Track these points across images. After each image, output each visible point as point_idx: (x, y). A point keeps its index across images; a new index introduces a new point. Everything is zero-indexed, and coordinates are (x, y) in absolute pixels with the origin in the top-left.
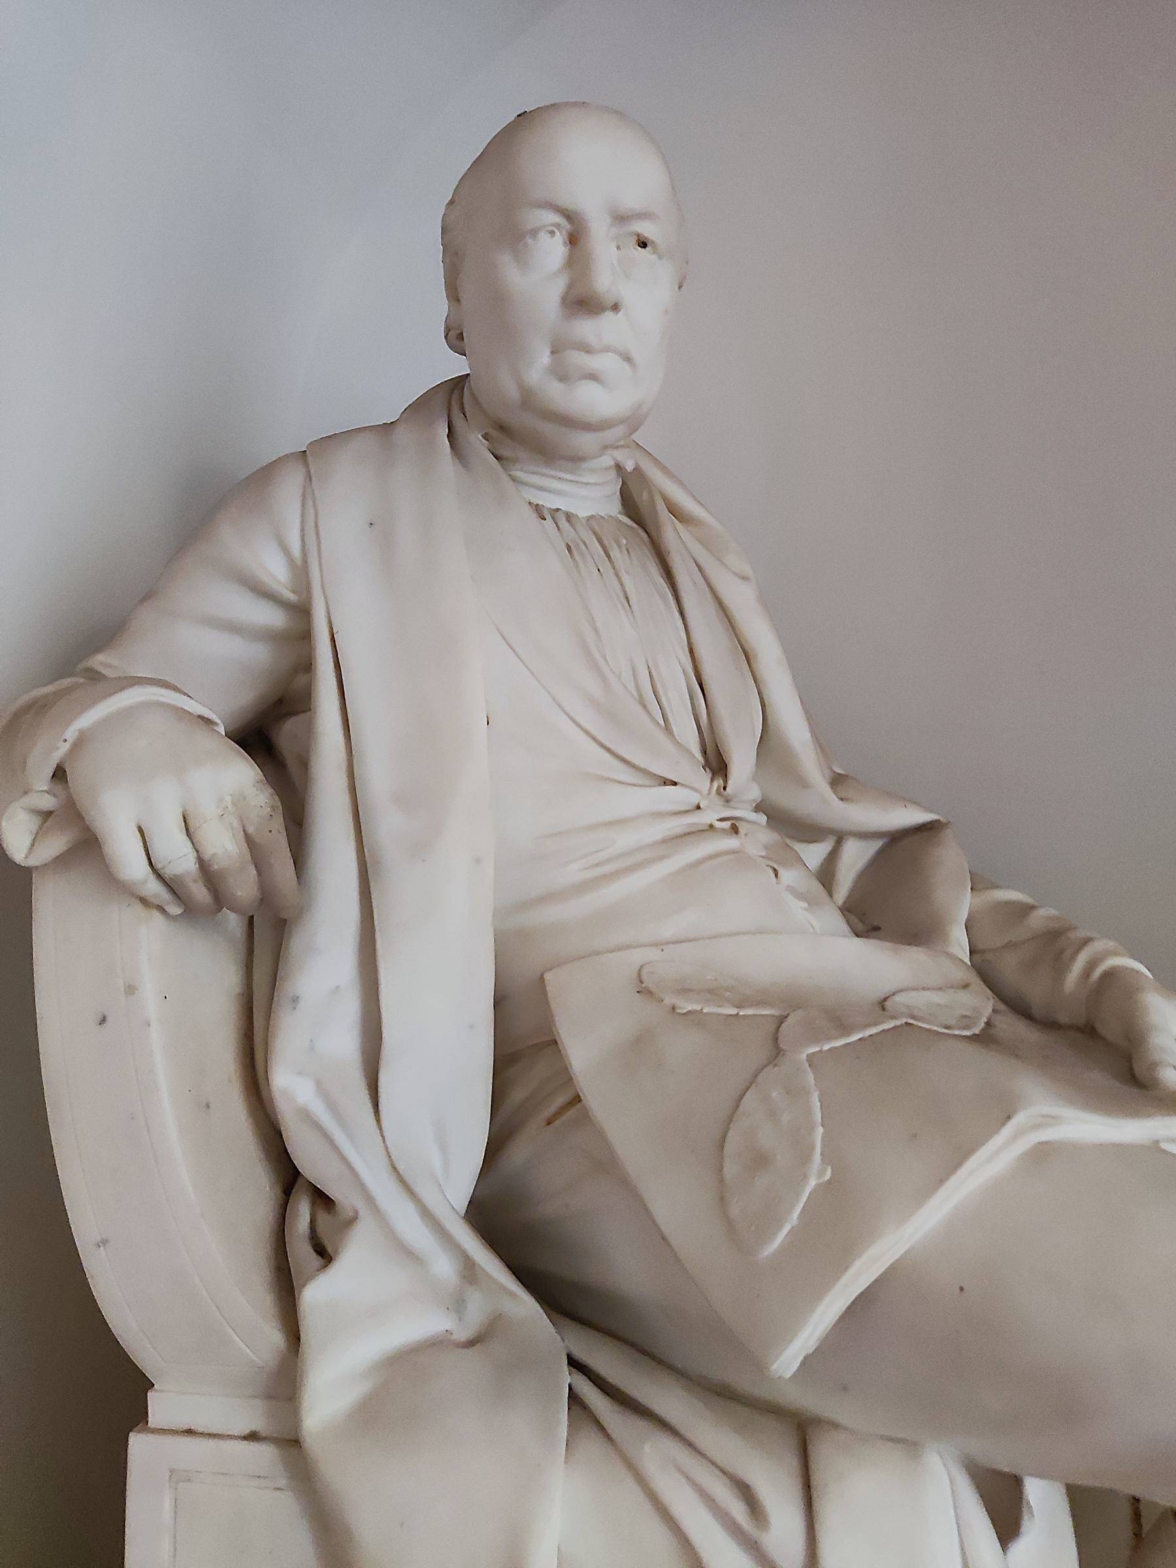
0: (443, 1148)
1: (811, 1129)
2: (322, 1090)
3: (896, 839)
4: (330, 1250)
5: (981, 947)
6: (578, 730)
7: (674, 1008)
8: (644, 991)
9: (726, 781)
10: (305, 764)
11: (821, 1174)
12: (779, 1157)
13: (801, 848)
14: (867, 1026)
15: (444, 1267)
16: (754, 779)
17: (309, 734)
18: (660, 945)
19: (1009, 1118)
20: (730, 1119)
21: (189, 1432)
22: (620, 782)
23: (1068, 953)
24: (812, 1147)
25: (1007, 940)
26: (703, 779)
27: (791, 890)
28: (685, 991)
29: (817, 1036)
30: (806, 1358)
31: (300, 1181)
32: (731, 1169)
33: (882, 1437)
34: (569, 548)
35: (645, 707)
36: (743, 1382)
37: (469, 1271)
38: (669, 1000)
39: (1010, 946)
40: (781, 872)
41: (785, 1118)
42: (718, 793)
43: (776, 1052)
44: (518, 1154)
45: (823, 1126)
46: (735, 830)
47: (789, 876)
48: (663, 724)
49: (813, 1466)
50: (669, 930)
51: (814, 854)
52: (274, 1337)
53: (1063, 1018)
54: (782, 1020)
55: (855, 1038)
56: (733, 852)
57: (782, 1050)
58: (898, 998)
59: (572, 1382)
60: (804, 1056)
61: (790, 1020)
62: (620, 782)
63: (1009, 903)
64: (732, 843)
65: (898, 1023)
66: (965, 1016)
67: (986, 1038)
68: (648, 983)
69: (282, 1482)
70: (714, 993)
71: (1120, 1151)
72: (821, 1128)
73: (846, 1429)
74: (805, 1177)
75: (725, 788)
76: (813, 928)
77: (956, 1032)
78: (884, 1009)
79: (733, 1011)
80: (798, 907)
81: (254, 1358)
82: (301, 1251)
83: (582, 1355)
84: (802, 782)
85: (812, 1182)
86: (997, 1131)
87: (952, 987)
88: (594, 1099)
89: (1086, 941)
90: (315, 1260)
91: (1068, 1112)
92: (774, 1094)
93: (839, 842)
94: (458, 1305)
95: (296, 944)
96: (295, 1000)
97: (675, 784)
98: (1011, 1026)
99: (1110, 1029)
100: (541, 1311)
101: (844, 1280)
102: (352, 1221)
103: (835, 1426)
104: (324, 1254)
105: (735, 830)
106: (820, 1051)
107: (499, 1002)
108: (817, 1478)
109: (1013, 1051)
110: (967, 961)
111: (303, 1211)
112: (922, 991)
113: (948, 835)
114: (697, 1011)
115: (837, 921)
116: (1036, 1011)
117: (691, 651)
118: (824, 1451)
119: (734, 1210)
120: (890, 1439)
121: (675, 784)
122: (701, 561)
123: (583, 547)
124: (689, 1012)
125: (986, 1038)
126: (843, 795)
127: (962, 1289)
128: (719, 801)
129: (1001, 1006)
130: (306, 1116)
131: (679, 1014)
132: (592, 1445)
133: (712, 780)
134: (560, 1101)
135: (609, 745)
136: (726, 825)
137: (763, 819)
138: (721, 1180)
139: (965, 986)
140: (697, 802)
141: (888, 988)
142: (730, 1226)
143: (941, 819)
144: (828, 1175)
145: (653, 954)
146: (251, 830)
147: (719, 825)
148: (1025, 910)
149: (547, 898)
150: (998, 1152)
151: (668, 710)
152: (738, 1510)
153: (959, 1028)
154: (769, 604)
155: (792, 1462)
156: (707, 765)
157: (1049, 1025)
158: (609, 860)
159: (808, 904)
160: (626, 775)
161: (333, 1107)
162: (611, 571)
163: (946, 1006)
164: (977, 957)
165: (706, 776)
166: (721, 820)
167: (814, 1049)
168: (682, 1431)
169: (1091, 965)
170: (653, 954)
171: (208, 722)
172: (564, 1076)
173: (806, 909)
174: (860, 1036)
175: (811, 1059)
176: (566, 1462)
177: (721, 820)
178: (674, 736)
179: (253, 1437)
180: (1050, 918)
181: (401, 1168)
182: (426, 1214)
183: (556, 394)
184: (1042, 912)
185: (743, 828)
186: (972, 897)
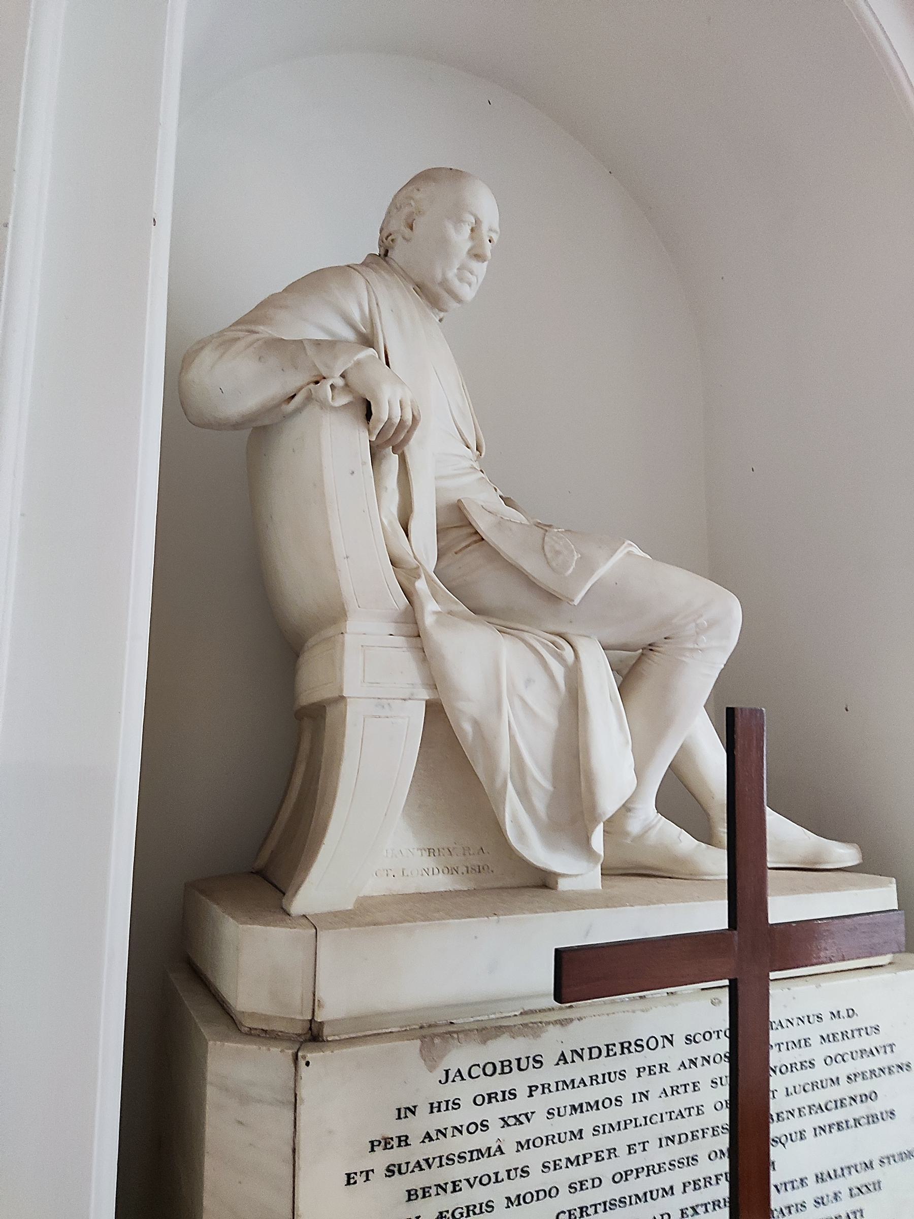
183: (456, 284)
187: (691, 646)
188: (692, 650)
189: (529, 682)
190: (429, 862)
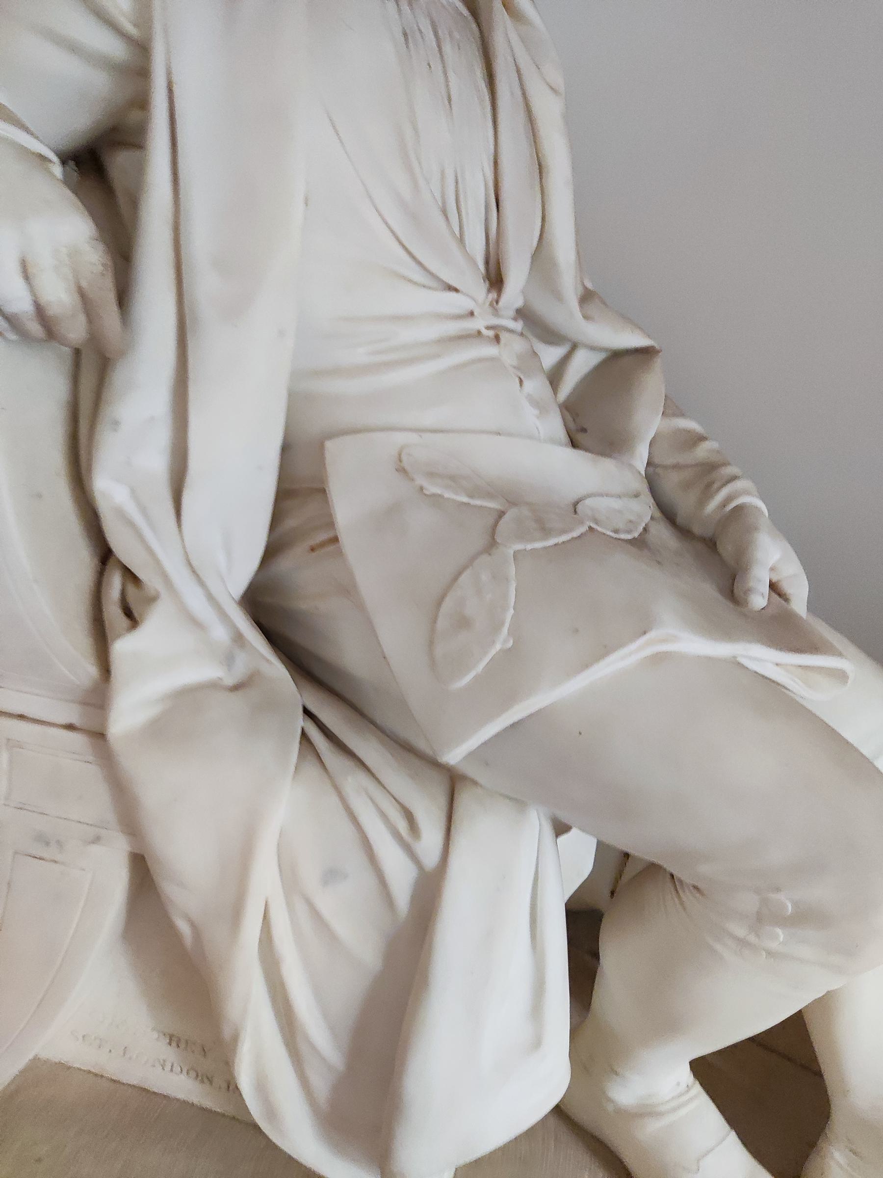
2: (133, 493)
3: (616, 356)
4: (136, 614)
5: (657, 460)
8: (402, 470)
9: (499, 295)
10: (135, 203)
11: (505, 641)
14: (564, 532)
15: (220, 634)
17: (140, 169)
19: (645, 633)
21: (21, 717)
22: (410, 281)
23: (715, 486)
24: (502, 623)
26: (479, 289)
29: (522, 535)
31: (111, 563)
32: (442, 623)
33: (502, 795)
34: (405, 35)
37: (238, 638)
39: (676, 467)
40: (526, 383)
42: (491, 305)
43: (492, 544)
44: (285, 564)
46: (497, 338)
50: (428, 419)
51: (550, 355)
52: (90, 670)
53: (697, 530)
54: (501, 514)
55: (552, 542)
56: (492, 359)
58: (588, 502)
61: (506, 517)
62: (410, 281)
63: (688, 432)
64: (491, 350)
67: (640, 543)
68: (406, 463)
69: (91, 758)
70: (453, 480)
71: (709, 660)
73: (481, 786)
74: (494, 642)
75: (497, 302)
78: (575, 512)
79: (464, 499)
80: (530, 413)
81: (72, 678)
84: (557, 295)
85: (498, 647)
88: (347, 541)
89: (733, 478)
90: (124, 621)
93: (574, 347)
94: (229, 660)
95: (119, 376)
96: (116, 423)
97: (456, 290)
98: (662, 533)
99: (726, 549)
102: (152, 599)
103: (475, 783)
104: (132, 617)
106: (525, 550)
107: (286, 449)
110: (643, 473)
111: (115, 583)
113: (658, 364)
116: (679, 520)
117: (496, 163)
118: (466, 800)
120: (510, 799)
121: (456, 290)
122: (522, 66)
123: (417, 33)
125: (640, 543)
127: (580, 733)
129: (658, 514)
130: (121, 514)
131: (425, 495)
132: (312, 770)
134: (322, 536)
135: (408, 246)
136: (491, 333)
139: (637, 496)
142: (433, 663)
143: (656, 345)
144: (510, 644)
146: (84, 284)
147: (485, 332)
148: (695, 439)
149: (337, 372)
151: (464, 220)
152: (402, 826)
154: (569, 120)
155: (442, 801)
160: (418, 275)
161: (144, 511)
162: (440, 67)
164: (651, 469)
167: (519, 546)
168: (374, 771)
171: (43, 158)
172: (331, 524)
176: (294, 777)
179: (70, 727)
181: (195, 563)
185: (504, 336)
186: (661, 420)
187: (740, 931)
188: (743, 943)
189: (331, 876)
190: (169, 1053)
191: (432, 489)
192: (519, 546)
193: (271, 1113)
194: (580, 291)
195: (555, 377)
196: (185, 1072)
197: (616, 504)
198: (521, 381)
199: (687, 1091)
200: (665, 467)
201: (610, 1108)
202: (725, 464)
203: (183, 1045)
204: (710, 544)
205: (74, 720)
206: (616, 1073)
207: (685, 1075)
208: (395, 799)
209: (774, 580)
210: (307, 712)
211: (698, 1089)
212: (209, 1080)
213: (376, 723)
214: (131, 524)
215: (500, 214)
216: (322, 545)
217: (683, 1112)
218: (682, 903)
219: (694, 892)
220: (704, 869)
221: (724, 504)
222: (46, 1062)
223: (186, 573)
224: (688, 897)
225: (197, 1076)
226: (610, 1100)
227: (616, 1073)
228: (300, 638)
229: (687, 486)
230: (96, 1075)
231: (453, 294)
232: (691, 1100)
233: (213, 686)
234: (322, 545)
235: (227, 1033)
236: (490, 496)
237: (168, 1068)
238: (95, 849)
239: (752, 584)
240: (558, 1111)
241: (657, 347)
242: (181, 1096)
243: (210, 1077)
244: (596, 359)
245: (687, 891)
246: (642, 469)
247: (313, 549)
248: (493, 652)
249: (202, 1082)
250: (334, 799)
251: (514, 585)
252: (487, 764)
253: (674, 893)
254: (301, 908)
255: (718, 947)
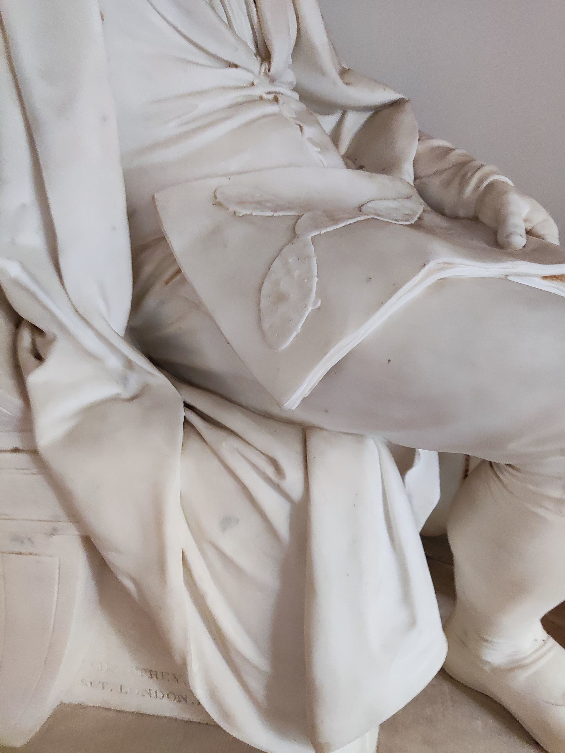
0: (105, 300)
1: (310, 279)
2: (24, 267)
4: (43, 356)
5: (421, 174)
6: (165, 23)
7: (235, 213)
8: (217, 204)
11: (315, 303)
12: (291, 296)
13: (321, 119)
16: (290, 67)
18: (228, 175)
20: (266, 275)
22: (197, 64)
23: (469, 174)
24: (310, 290)
25: (435, 170)
26: (255, 63)
27: (310, 139)
28: (242, 203)
30: (304, 398)
32: (264, 303)
35: (213, 8)
36: (275, 410)
37: (129, 365)
38: (232, 208)
40: (305, 128)
41: (297, 273)
42: (265, 74)
43: (294, 235)
45: (317, 277)
46: (276, 100)
47: (310, 131)
48: (227, 22)
49: (308, 448)
50: (233, 165)
52: (17, 402)
54: (299, 217)
56: (275, 115)
57: (297, 234)
58: (369, 205)
59: (186, 415)
60: (310, 238)
62: (197, 64)
63: (439, 147)
64: (273, 109)
65: (368, 217)
66: (407, 215)
68: (220, 198)
69: (35, 471)
70: (260, 204)
71: (483, 281)
72: (317, 278)
73: (326, 430)
75: (269, 70)
76: (323, 165)
77: (402, 223)
78: (360, 211)
79: (270, 214)
80: (314, 151)
82: (25, 356)
83: (190, 402)
84: (321, 71)
85: (310, 309)
86: (415, 274)
87: (402, 198)
89: (481, 166)
90: (33, 360)
91: (459, 260)
92: (291, 260)
94: (124, 380)
98: (433, 219)
99: (486, 217)
100: (169, 382)
101: (324, 360)
102: (53, 340)
103: (321, 429)
104: (39, 357)
105: (276, 100)
106: (320, 234)
108: (310, 455)
109: (431, 231)
110: (413, 184)
112: (384, 201)
114: (248, 215)
115: (339, 161)
116: (447, 211)
118: (315, 442)
119: (266, 325)
121: (236, 66)
124: (244, 215)
125: (418, 226)
126: (347, 81)
127: (389, 361)
128: (266, 81)
129: (429, 209)
131: (239, 217)
132: (195, 444)
133: (261, 64)
136: (271, 97)
137: (296, 96)
138: (259, 310)
139: (409, 197)
140: (252, 81)
141: (363, 200)
145: (224, 181)
147: (266, 96)
148: (448, 151)
150: (416, 285)
151: (232, 18)
152: (270, 471)
153: (402, 221)
155: (298, 448)
156: (258, 54)
157: (454, 218)
158: (194, 120)
159: (321, 149)
160: (202, 59)
163: (397, 209)
164: (417, 181)
165: (257, 61)
166: (268, 93)
167: (316, 233)
168: (244, 437)
169: (481, 181)
170: (224, 181)
172: (170, 257)
173: (319, 152)
174: (344, 224)
175: (313, 239)
177: (268, 93)
178: (235, 31)
179: (16, 450)
180: (463, 155)
181: (81, 311)
182: (100, 336)
184: (457, 152)
190: (152, 685)
191: (243, 212)
192: (316, 233)
193: (226, 715)
194: (339, 68)
195: (335, 137)
196: (166, 696)
197: (392, 204)
198: (301, 128)
199: (544, 645)
200: (428, 176)
201: (487, 668)
202: (473, 160)
203: (160, 676)
204: (475, 219)
205: (18, 445)
206: (486, 641)
207: (540, 632)
208: (262, 453)
209: (529, 228)
210: (187, 406)
211: (552, 642)
212: (184, 699)
213: (243, 405)
214: (26, 290)
215: (258, 6)
216: (172, 277)
217: (543, 662)
218: (501, 481)
219: (508, 468)
220: (513, 446)
221: (478, 187)
222: (70, 705)
223: (76, 319)
224: (506, 477)
225: (175, 698)
226: (486, 663)
227: (486, 641)
228: (177, 358)
229: (447, 184)
230: (105, 709)
231: (233, 70)
232: (549, 650)
233: (115, 399)
234: (172, 277)
235: (178, 658)
236: (289, 208)
237: (153, 695)
238: (55, 538)
239: (510, 229)
240: (444, 673)
241: (406, 98)
242: (168, 714)
243: (184, 697)
244: (364, 117)
245: (506, 473)
246: (411, 181)
247: (167, 283)
248: (307, 313)
249: (179, 701)
250: (215, 463)
251: (315, 259)
252: (327, 411)
253: (496, 479)
254: (210, 551)
255: (541, 512)
